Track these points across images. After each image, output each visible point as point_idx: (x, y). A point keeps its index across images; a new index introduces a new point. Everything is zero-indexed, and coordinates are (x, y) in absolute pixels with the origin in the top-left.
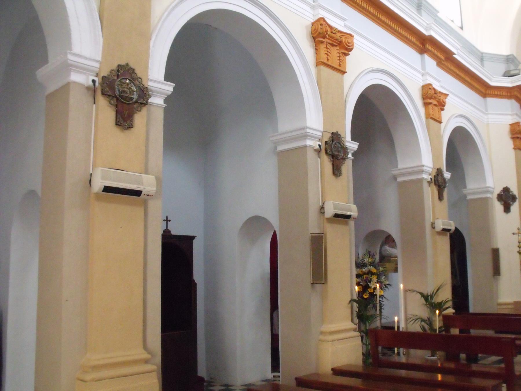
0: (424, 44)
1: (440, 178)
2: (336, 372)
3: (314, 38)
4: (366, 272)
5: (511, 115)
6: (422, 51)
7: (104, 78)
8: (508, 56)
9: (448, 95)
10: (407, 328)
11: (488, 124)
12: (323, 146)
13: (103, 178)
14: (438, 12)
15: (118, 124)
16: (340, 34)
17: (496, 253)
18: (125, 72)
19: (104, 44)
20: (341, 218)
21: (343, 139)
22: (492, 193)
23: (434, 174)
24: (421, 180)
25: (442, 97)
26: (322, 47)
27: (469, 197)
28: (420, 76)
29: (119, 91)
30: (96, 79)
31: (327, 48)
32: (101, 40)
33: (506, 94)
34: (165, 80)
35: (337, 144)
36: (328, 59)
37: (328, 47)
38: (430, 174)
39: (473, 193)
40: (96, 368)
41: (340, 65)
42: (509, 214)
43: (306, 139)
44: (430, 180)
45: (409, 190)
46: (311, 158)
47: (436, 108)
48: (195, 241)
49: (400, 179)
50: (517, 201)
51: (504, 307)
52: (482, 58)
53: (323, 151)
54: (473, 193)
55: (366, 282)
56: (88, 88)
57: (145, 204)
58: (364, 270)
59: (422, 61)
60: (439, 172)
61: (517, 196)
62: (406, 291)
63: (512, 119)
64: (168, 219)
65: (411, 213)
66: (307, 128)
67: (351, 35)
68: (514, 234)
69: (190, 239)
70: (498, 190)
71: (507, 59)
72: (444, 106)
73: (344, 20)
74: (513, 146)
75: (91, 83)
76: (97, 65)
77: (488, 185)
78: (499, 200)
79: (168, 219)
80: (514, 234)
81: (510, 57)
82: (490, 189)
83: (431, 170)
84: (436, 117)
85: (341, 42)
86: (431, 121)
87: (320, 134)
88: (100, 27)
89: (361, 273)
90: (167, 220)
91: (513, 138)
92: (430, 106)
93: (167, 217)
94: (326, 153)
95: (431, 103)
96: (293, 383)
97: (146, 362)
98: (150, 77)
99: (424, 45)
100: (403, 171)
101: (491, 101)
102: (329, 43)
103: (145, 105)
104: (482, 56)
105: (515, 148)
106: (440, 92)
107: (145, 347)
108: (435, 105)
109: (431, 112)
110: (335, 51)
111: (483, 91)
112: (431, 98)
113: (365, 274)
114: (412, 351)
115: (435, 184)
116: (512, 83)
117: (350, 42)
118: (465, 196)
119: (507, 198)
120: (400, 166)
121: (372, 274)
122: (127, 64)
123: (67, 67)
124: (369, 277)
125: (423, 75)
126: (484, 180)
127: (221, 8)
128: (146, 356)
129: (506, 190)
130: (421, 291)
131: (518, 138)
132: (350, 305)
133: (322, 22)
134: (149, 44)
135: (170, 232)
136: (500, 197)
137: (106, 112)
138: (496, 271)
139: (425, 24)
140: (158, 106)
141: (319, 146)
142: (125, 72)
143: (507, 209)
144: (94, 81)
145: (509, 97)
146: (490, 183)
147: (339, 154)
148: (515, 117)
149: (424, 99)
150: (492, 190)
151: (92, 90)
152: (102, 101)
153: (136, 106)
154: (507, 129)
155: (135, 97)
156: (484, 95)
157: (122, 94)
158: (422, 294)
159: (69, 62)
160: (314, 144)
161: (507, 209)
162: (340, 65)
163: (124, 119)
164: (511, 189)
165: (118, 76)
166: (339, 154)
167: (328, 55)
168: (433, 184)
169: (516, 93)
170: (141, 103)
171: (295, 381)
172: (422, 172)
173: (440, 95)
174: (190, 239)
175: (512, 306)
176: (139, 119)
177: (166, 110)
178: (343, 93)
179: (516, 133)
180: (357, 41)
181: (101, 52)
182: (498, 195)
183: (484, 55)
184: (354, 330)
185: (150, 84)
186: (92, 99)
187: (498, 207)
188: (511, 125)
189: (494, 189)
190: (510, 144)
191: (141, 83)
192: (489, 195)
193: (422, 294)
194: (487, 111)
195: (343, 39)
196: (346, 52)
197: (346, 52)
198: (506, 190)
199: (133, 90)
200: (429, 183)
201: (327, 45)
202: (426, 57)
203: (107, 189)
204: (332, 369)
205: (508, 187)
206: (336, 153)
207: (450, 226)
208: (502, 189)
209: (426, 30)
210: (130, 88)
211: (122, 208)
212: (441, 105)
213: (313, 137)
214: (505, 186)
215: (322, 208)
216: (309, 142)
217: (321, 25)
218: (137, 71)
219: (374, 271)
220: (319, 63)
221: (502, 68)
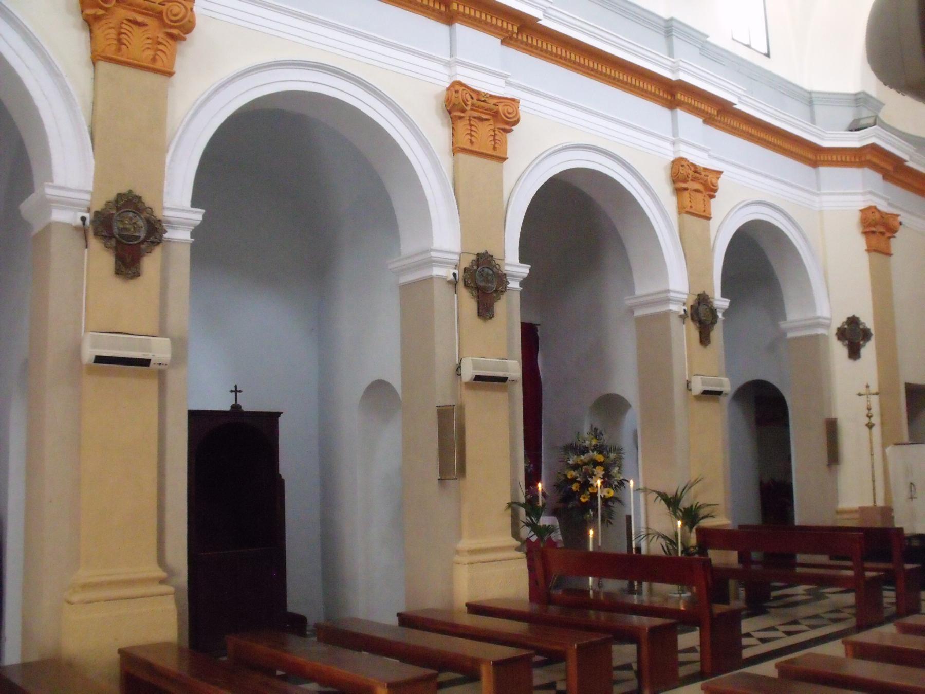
0: (671, 93)
1: (702, 309)
2: (475, 609)
3: (450, 112)
4: (586, 461)
5: (863, 194)
6: (672, 104)
7: (97, 213)
8: (856, 94)
9: (721, 172)
10: (648, 549)
11: (821, 211)
12: (460, 275)
13: (94, 346)
14: (707, 36)
15: (118, 272)
16: (495, 101)
17: (832, 428)
18: (129, 203)
19: (96, 167)
20: (487, 381)
21: (497, 261)
22: (828, 326)
23: (691, 303)
24: (667, 315)
25: (711, 178)
26: (462, 126)
27: (790, 335)
28: (668, 145)
29: (118, 228)
30: (87, 215)
31: (471, 125)
32: (92, 163)
33: (853, 160)
34: (192, 206)
35: (486, 270)
36: (472, 142)
37: (472, 123)
38: (684, 304)
39: (797, 328)
40: (85, 587)
41: (495, 148)
42: (858, 362)
43: (432, 266)
44: (683, 312)
45: (652, 327)
46: (441, 294)
47: (700, 197)
48: (281, 420)
49: (639, 313)
50: (873, 339)
51: (846, 516)
52: (809, 100)
53: (461, 284)
54: (797, 328)
55: (585, 477)
56: (76, 228)
57: (161, 375)
58: (582, 457)
59: (672, 120)
60: (703, 300)
61: (873, 331)
62: (637, 490)
63: (861, 202)
64: (234, 389)
65: (655, 367)
66: (432, 250)
67: (513, 100)
68: (860, 395)
69: (272, 418)
70: (839, 321)
71: (856, 100)
72: (715, 191)
73: (505, 77)
74: (866, 247)
75: (79, 222)
76: (88, 197)
77: (819, 314)
78: (839, 339)
79: (234, 389)
80: (860, 395)
81: (859, 96)
82: (820, 320)
83: (686, 296)
84: (699, 208)
85: (497, 112)
86: (687, 217)
87: (457, 257)
88: (90, 145)
89: (579, 462)
90: (236, 391)
91: (866, 233)
92: (686, 194)
93: (236, 387)
94: (466, 285)
95: (686, 189)
96: (394, 621)
97: (162, 581)
98: (166, 205)
99: (673, 95)
100: (641, 299)
101: (824, 170)
102: (475, 118)
103: (159, 243)
104: (811, 98)
105: (870, 250)
106: (705, 169)
107: (161, 560)
108: (697, 191)
109: (687, 203)
110: (484, 131)
111: (811, 156)
112: (685, 181)
113: (585, 464)
114: (658, 586)
115: (693, 319)
116: (860, 140)
117: (510, 110)
118: (784, 334)
119: (853, 335)
120: (639, 291)
121: (596, 464)
122: (130, 191)
123: (47, 205)
124: (590, 467)
125: (674, 143)
126: (812, 305)
127: (229, 115)
128: (162, 574)
129: (853, 321)
130: (661, 490)
131: (873, 232)
132: (509, 511)
133: (457, 87)
134: (165, 158)
135: (240, 407)
136: (842, 334)
137: (101, 259)
138: (833, 456)
139: (669, 63)
140: (181, 242)
141: (454, 275)
142: (129, 203)
143: (854, 353)
144: (83, 219)
145: (861, 164)
146: (823, 310)
147: (490, 285)
148: (869, 197)
149: (674, 182)
150: (828, 321)
151: (82, 230)
152: (95, 244)
153: (143, 246)
154: (856, 218)
155: (142, 235)
156: (814, 164)
157: (126, 232)
158: (663, 496)
159: (48, 197)
160: (448, 273)
161: (854, 353)
162: (495, 148)
163: (128, 262)
164: (862, 320)
165: (118, 209)
166: (490, 285)
167: (471, 135)
168: (689, 320)
169: (869, 157)
170: (152, 242)
171: (397, 618)
172: (668, 301)
173: (706, 173)
174: (272, 418)
175: (857, 516)
176: (151, 263)
177: (193, 246)
178: (501, 191)
179: (870, 225)
180: (528, 106)
181: (92, 180)
182: (839, 329)
183: (813, 95)
184: (518, 549)
185: (167, 213)
186: (83, 241)
187: (839, 350)
188: (861, 211)
189: (831, 319)
190: (861, 243)
191: (152, 213)
192: (820, 331)
193: (663, 496)
194: (819, 189)
195: (501, 108)
196: (507, 127)
197: (507, 127)
198: (853, 321)
199: (138, 226)
200: (683, 317)
201: (470, 120)
202: (681, 113)
203: (99, 359)
204: (467, 605)
205: (857, 315)
206: (483, 284)
207: (721, 385)
208: (845, 320)
209: (673, 72)
210: (135, 223)
211: (126, 380)
212: (711, 191)
213: (442, 263)
214: (850, 315)
215: (459, 367)
216: (437, 271)
217: (457, 92)
218: (144, 200)
219: (600, 458)
220: (457, 150)
221: (847, 115)
